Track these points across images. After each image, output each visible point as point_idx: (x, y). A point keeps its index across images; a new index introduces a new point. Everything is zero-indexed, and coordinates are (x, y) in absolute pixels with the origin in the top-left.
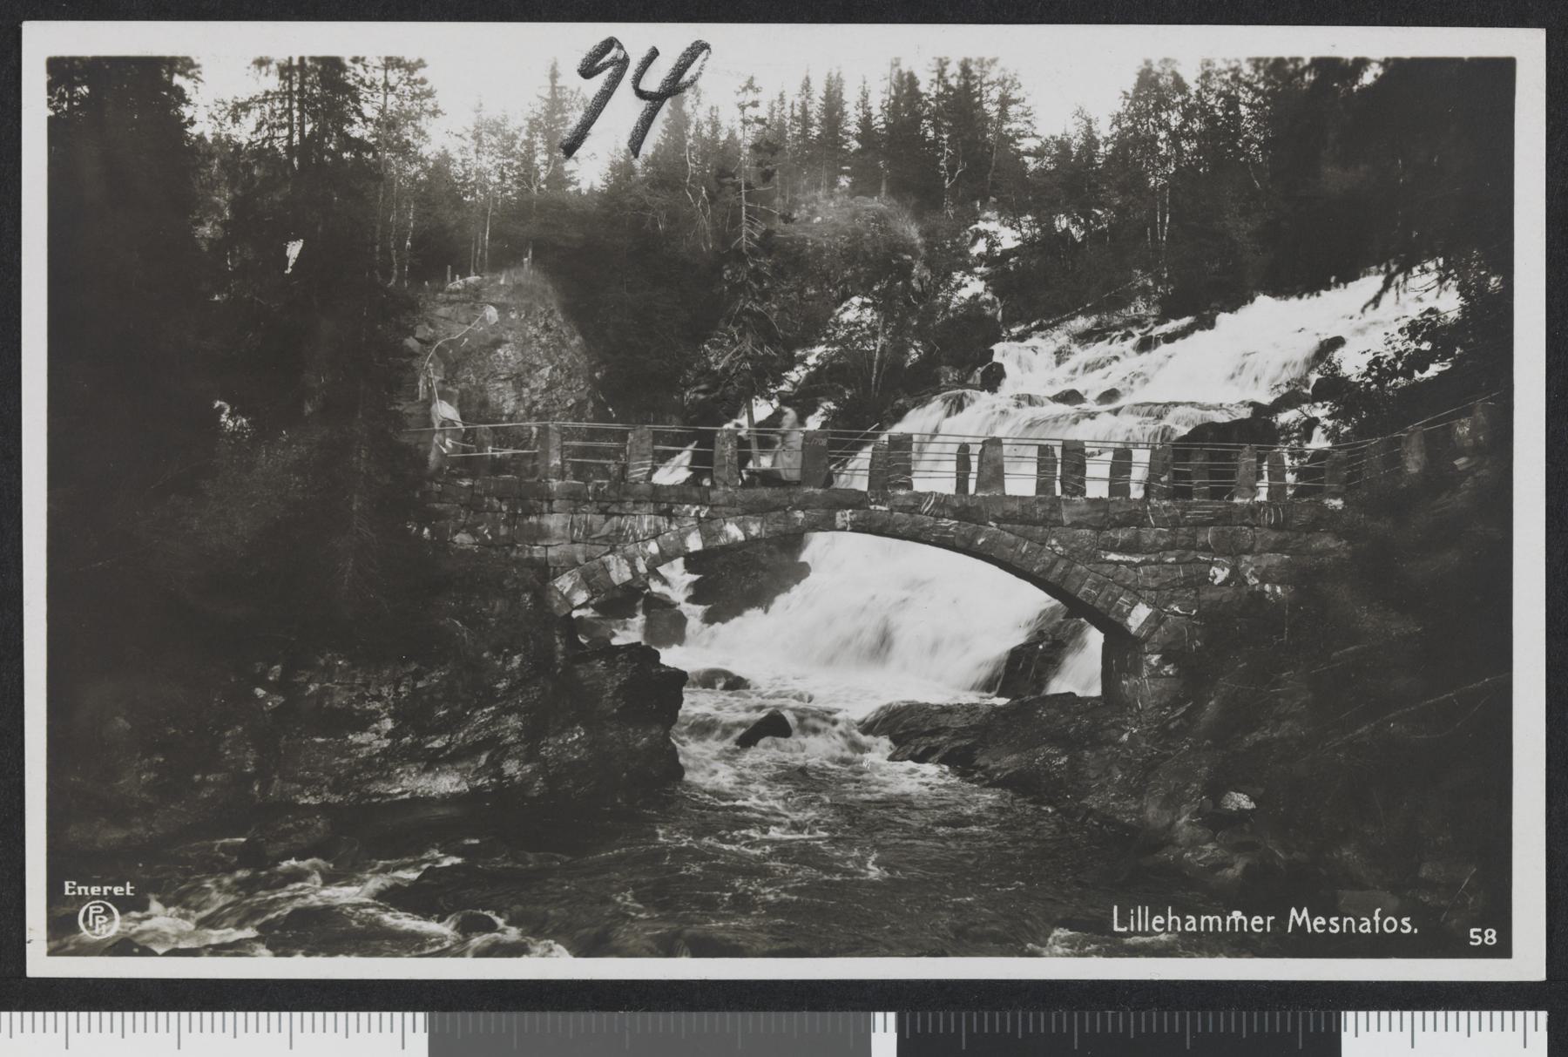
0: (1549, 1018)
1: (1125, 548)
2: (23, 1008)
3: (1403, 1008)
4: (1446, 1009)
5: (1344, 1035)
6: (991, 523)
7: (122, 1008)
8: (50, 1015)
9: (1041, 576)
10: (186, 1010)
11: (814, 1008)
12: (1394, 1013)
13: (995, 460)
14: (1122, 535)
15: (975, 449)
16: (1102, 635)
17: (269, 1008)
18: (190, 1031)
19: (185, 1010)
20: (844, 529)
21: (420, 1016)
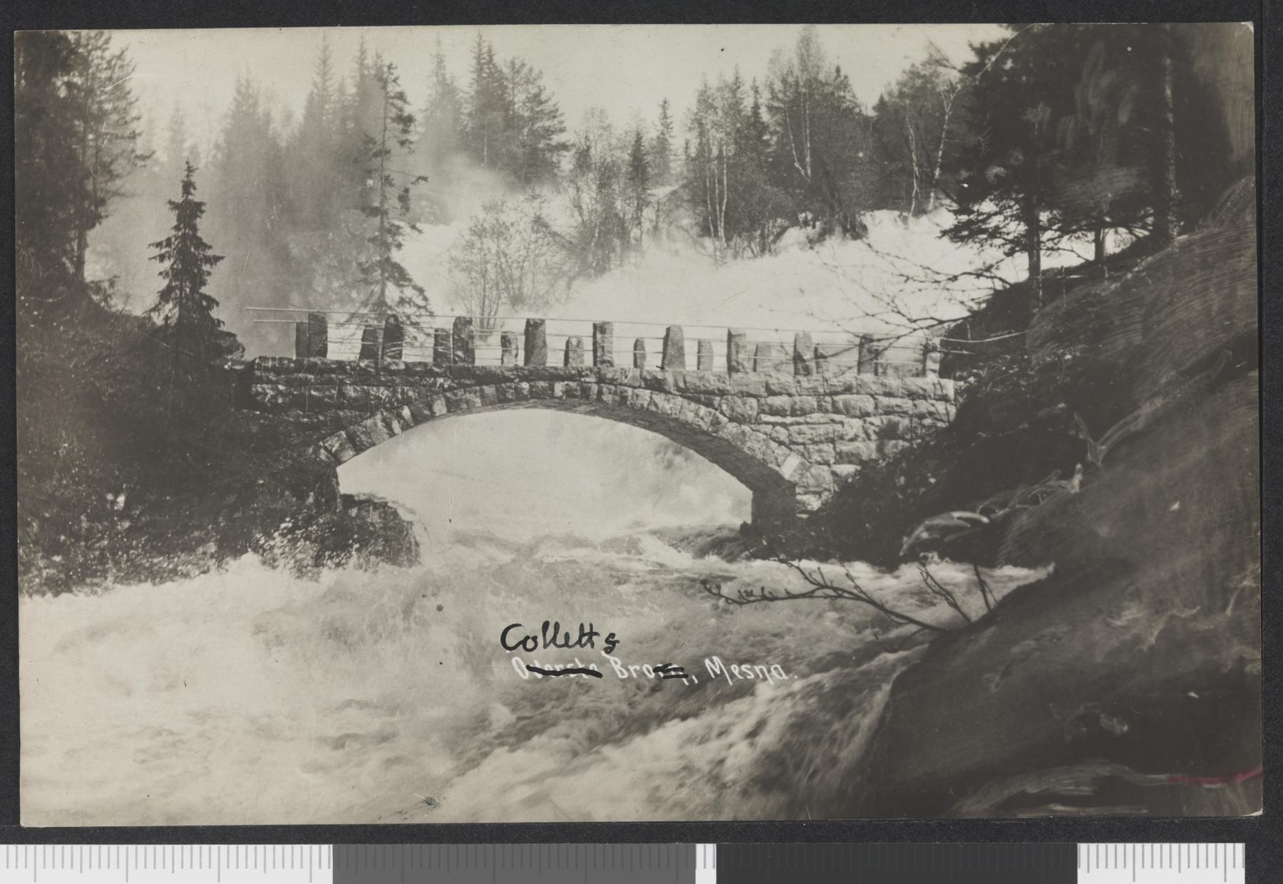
16: (751, 492)
18: (1189, 867)
19: (1148, 841)
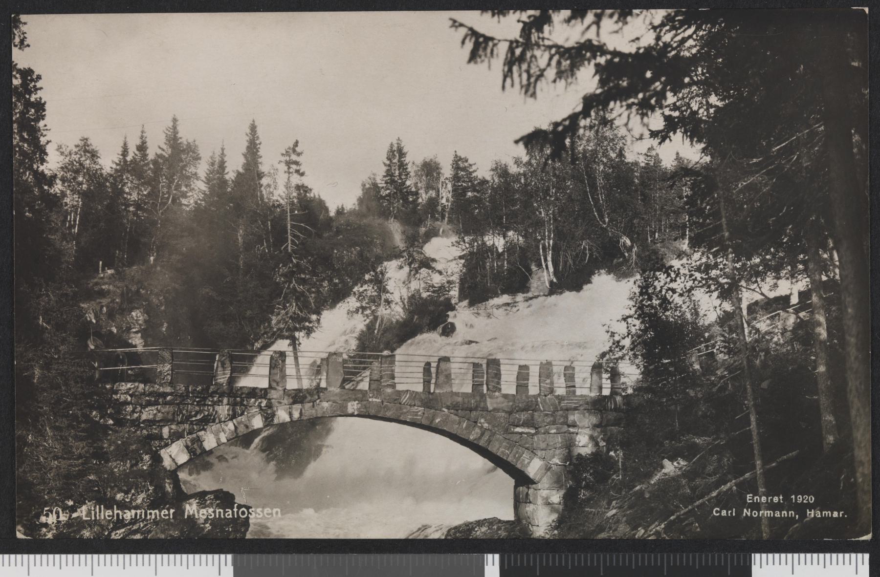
1: (526, 424)
6: (444, 409)
7: (194, 552)
9: (475, 442)
10: (192, 553)
12: (152, 555)
13: (446, 370)
14: (523, 416)
15: (434, 365)
20: (352, 415)
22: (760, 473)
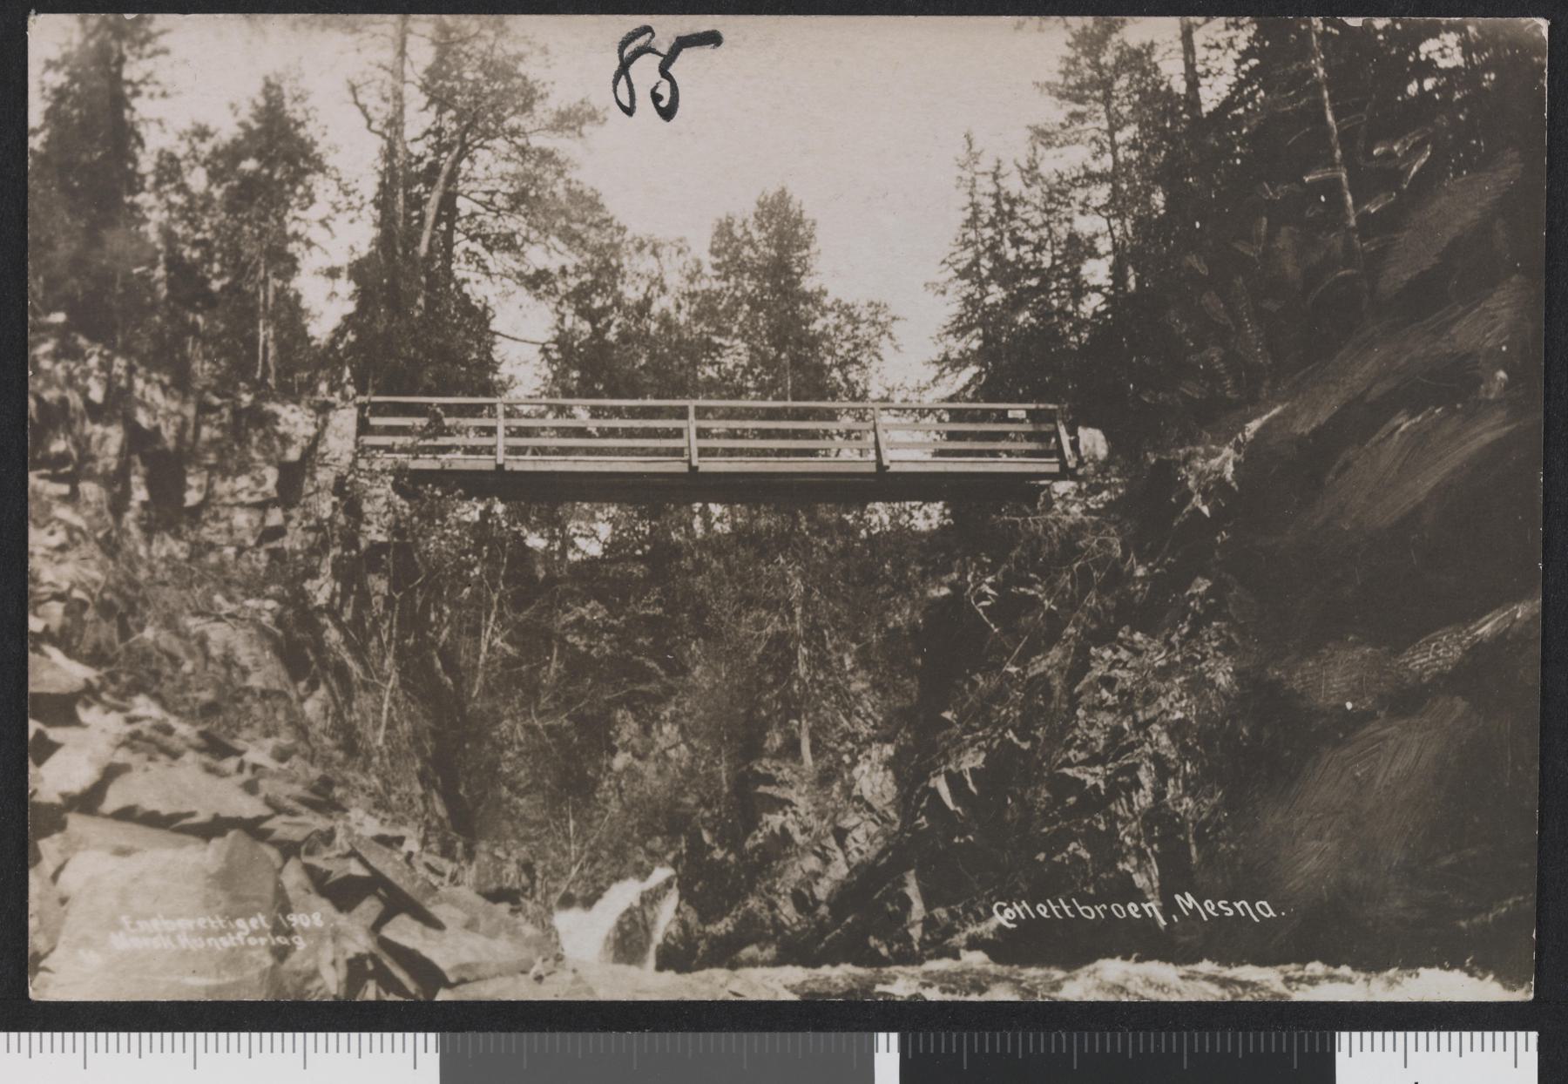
0: (1539, 1038)
2: (42, 1029)
3: (1385, 1028)
4: (1439, 1030)
5: (1338, 1055)
7: (139, 1029)
8: (69, 1035)
11: (818, 1028)
12: (309, 1035)
17: (74, 1028)
21: (432, 1037)
22: (1000, 928)
